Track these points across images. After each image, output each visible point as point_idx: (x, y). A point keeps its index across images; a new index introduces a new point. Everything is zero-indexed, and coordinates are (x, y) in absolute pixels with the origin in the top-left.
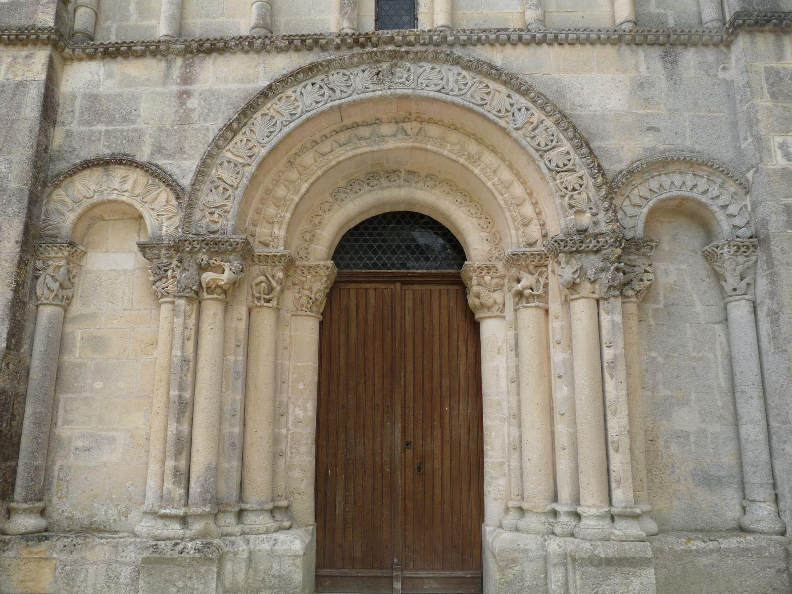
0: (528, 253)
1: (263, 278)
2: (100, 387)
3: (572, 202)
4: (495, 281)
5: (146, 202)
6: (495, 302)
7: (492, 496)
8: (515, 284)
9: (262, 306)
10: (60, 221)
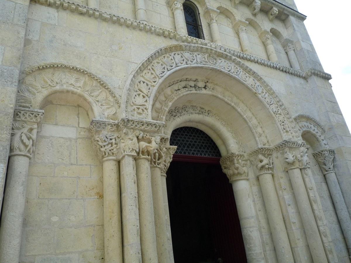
0: (266, 148)
2: (56, 220)
4: (243, 162)
5: (93, 96)
6: (244, 172)
8: (259, 163)
9: (156, 167)
10: (32, 98)
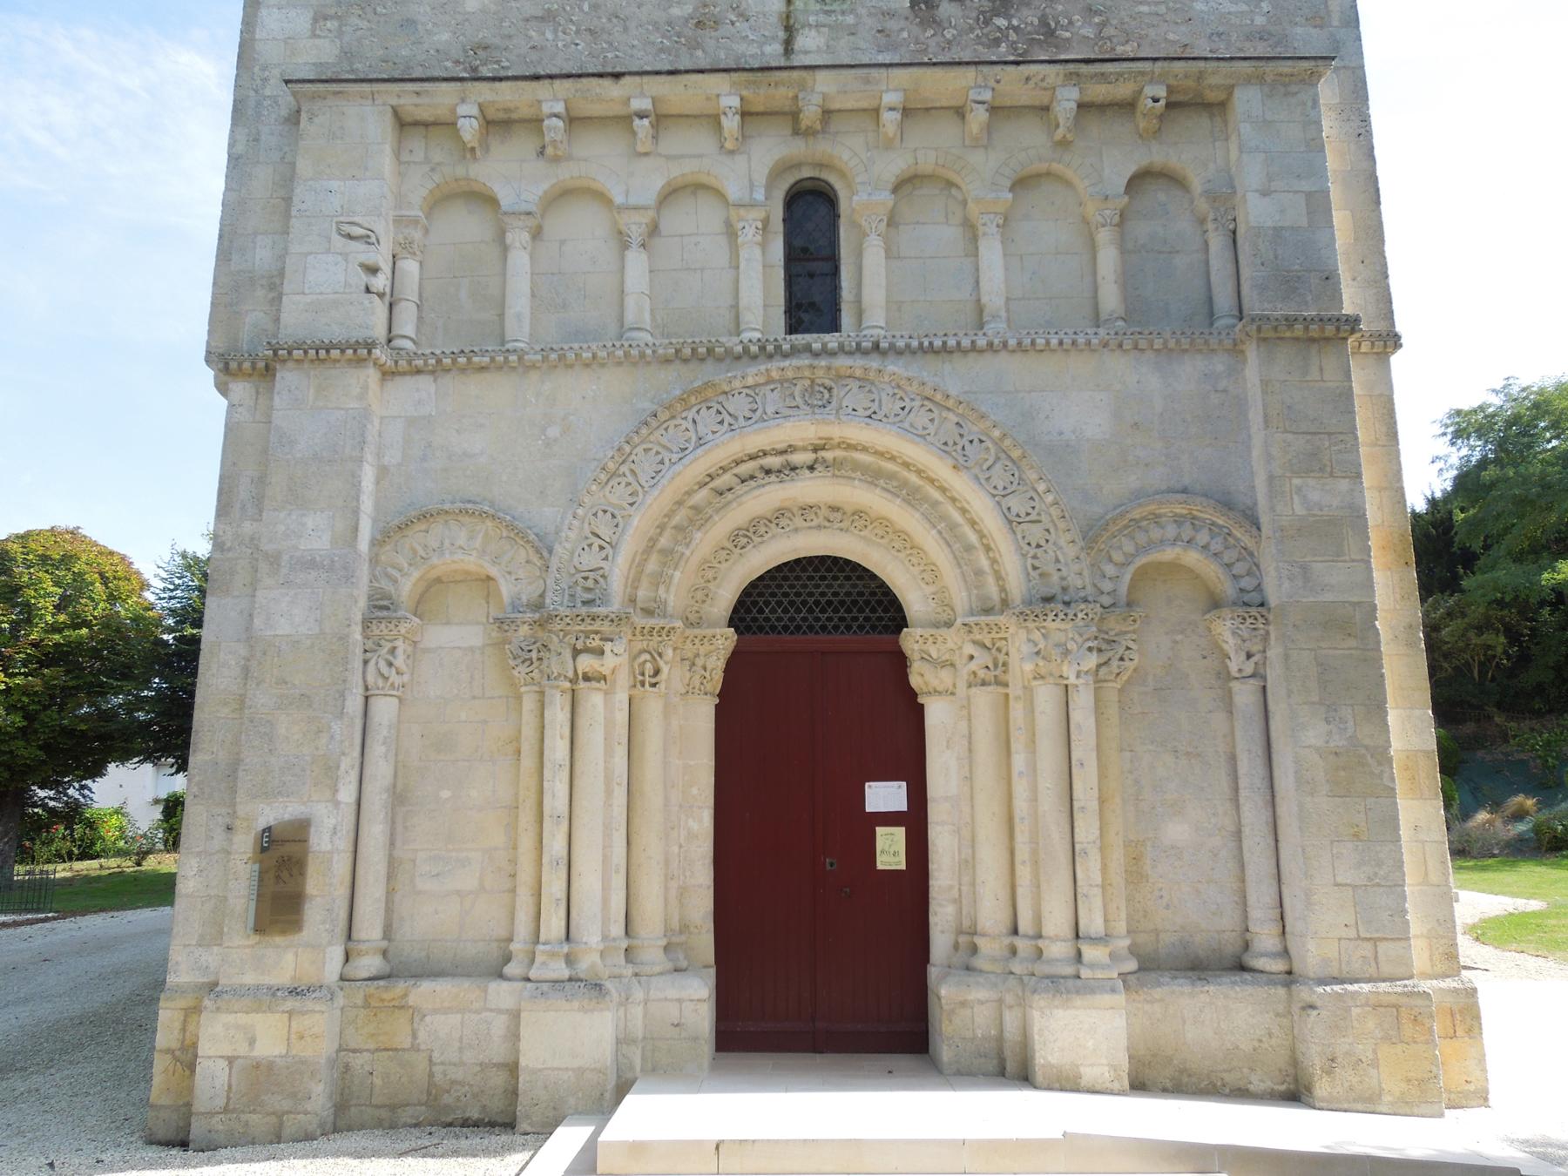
1: (647, 657)
3: (1037, 563)
7: (939, 928)
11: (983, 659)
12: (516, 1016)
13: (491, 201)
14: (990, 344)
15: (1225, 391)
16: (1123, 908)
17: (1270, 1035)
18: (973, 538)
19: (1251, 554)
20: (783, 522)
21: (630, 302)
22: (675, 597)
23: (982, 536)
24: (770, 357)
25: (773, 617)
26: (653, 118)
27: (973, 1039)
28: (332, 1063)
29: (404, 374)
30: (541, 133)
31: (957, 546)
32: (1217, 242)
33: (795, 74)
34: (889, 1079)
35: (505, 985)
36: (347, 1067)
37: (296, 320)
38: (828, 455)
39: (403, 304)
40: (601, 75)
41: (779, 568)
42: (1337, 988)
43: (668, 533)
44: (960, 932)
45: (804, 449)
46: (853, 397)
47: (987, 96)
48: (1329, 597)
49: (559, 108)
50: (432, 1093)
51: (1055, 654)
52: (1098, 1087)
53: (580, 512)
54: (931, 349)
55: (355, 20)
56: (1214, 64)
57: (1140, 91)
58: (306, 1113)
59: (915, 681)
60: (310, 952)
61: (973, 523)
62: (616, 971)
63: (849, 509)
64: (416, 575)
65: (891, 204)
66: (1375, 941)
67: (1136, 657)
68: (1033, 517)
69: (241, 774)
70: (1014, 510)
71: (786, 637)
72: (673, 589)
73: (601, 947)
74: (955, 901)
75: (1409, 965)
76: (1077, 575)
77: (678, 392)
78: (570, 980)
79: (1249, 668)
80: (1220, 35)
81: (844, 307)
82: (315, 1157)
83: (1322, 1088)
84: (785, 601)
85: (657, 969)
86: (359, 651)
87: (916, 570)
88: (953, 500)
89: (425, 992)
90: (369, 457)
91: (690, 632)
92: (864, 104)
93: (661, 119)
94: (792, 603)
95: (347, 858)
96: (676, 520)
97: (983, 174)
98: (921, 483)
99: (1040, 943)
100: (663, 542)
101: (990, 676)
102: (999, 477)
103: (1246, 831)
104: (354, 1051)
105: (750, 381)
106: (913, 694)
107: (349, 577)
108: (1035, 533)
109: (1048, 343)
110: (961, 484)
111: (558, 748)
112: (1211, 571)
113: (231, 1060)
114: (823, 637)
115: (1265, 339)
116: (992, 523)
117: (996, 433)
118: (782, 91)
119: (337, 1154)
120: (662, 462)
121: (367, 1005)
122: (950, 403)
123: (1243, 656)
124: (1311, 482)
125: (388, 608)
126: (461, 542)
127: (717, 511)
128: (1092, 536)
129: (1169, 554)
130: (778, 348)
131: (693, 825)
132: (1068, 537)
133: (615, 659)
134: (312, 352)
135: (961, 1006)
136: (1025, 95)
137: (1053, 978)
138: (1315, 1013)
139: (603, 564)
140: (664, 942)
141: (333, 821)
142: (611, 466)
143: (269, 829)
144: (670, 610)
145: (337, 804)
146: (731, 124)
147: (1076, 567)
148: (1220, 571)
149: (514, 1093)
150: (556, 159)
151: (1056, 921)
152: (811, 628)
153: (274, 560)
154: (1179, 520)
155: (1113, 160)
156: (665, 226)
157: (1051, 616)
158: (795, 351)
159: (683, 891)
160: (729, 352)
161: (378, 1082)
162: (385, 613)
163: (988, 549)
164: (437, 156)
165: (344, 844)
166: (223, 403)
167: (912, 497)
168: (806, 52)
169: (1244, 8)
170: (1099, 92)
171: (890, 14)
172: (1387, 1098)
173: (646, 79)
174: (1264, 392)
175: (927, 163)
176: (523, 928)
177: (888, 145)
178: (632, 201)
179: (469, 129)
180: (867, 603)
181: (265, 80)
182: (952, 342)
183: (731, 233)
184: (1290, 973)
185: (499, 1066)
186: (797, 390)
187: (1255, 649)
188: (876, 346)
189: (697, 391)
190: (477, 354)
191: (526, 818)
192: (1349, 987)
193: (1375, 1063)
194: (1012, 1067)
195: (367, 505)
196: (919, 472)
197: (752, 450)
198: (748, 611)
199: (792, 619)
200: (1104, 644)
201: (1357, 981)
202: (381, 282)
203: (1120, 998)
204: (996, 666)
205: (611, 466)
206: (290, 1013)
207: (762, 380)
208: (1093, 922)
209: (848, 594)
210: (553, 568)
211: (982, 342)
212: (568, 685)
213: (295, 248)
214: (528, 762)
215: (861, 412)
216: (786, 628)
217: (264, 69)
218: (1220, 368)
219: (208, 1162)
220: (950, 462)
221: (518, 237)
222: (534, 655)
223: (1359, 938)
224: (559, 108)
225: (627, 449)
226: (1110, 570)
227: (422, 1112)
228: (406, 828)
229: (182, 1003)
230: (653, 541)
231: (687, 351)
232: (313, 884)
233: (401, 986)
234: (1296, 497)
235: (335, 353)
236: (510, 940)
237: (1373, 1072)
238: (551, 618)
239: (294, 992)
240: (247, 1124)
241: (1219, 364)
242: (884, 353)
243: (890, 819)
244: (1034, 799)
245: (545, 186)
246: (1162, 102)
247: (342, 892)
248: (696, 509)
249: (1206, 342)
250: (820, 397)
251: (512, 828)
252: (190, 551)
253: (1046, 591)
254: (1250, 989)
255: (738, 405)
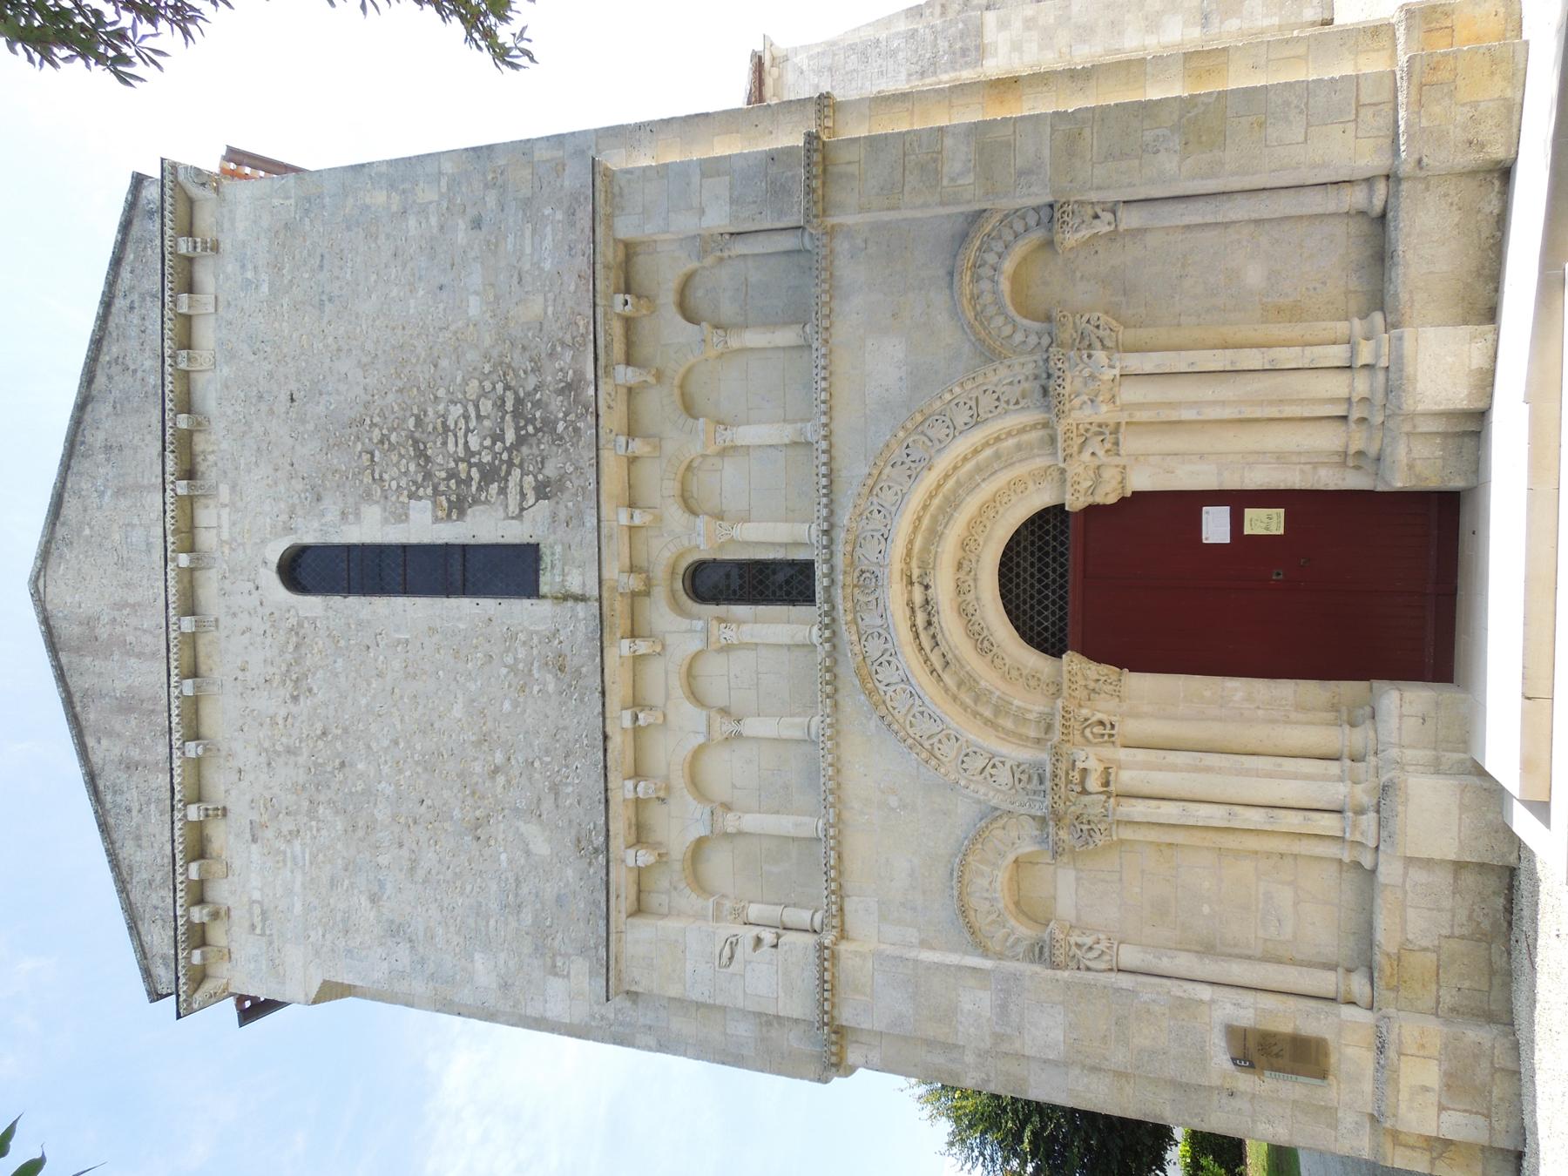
11: (1094, 445)
12: (1410, 861)
13: (700, 843)
14: (825, 437)
15: (866, 241)
16: (1323, 324)
17: (1446, 195)
18: (988, 452)
19: (1006, 216)
20: (970, 610)
21: (786, 734)
22: (1035, 705)
23: (987, 444)
24: (833, 620)
25: (1051, 619)
26: (637, 710)
27: (1443, 458)
28: (1447, 1022)
29: (843, 922)
30: (646, 801)
31: (996, 466)
32: (740, 248)
33: (605, 595)
34: (1479, 532)
35: (1381, 869)
36: (1453, 1010)
37: (799, 1005)
38: (916, 573)
39: (785, 918)
40: (605, 750)
41: (1009, 613)
42: (1402, 140)
43: (981, 709)
44: (1344, 464)
45: (910, 592)
46: (869, 552)
47: (622, 440)
48: (1046, 152)
49: (630, 784)
50: (1481, 937)
51: (1093, 386)
52: (1491, 353)
53: (963, 783)
54: (829, 486)
55: (556, 943)
56: (598, 256)
57: (618, 315)
58: (1493, 1047)
59: (1112, 499)
60: (1347, 1034)
61: (976, 452)
62: (1372, 771)
63: (960, 554)
64: (1013, 922)
65: (706, 518)
66: (1359, 106)
67: (1095, 315)
68: (973, 404)
69: (1184, 1080)
70: (968, 420)
71: (1069, 608)
72: (1029, 707)
73: (1349, 783)
74: (1315, 468)
75: (1381, 75)
76: (1024, 367)
77: (863, 697)
78: (1378, 812)
79: (1108, 216)
80: (571, 249)
81: (790, 557)
82: (1533, 1041)
83: (1498, 152)
84: (1037, 608)
85: (1371, 734)
86: (1079, 974)
87: (1014, 498)
88: (955, 468)
89: (1386, 936)
90: (912, 954)
91: (1065, 693)
92: (626, 538)
93: (637, 703)
94: (1039, 602)
95: (1262, 997)
96: (969, 701)
97: (687, 442)
98: (940, 496)
99: (1355, 399)
100: (988, 713)
101: (1110, 438)
102: (939, 432)
103: (1255, 216)
104: (1438, 1002)
105: (855, 638)
106: (1123, 500)
107: (1016, 977)
108: (987, 401)
109: (824, 390)
110: (943, 463)
111: (1169, 812)
112: (1020, 249)
113: (1442, 1108)
114: (1070, 577)
115: (824, 211)
116: (977, 436)
117: (901, 434)
118: (617, 605)
119: (1532, 1023)
120: (922, 713)
121: (1396, 989)
122: (875, 472)
123: (1096, 222)
124: (946, 169)
125: (1042, 948)
126: (985, 883)
127: (962, 667)
128: (989, 353)
129: (1005, 286)
130: (827, 614)
131: (1239, 695)
132: (990, 374)
133: (1091, 758)
134: (826, 994)
135: (1413, 466)
136: (621, 407)
137: (1388, 391)
138: (1425, 160)
139: (1008, 766)
140: (1347, 727)
141: (1228, 1006)
142: (924, 755)
143: (1234, 1060)
144: (1047, 710)
145: (1212, 1001)
146: (643, 647)
147: (1017, 368)
148: (1020, 243)
149: (1482, 865)
150: (668, 789)
151: (1336, 385)
152: (1062, 587)
153: (999, 1038)
154: (976, 279)
155: (671, 334)
156: (722, 703)
157: (1060, 390)
158: (829, 600)
159: (1299, 707)
160: (829, 655)
161: (1467, 984)
162: (1046, 950)
163: (998, 439)
164: (664, 883)
165: (1249, 998)
166: (861, 1071)
167: (952, 503)
168: (584, 584)
169: (549, 228)
170: (618, 349)
171: (554, 515)
172: (1509, 93)
173: (608, 715)
174: (869, 210)
175: (672, 487)
176: (1332, 850)
177: (659, 519)
178: (703, 728)
179: (645, 857)
180: (1040, 538)
181: (602, 1018)
182: (823, 470)
183: (727, 649)
184: (1388, 177)
185: (1456, 879)
186: (863, 599)
187: (1090, 212)
188: (826, 532)
189: (863, 682)
190: (828, 861)
191: (1230, 841)
192: (1402, 128)
193: (1475, 105)
194: (1471, 427)
195: (953, 959)
196: (931, 497)
197: (911, 636)
198: (1046, 640)
199: (1054, 603)
200: (1085, 344)
201: (1396, 122)
202: (768, 936)
203: (1408, 332)
204: (1101, 433)
205: (924, 755)
206: (1400, 1054)
207: (854, 629)
208: (1338, 354)
209: (1032, 554)
210: (1011, 808)
211: (824, 445)
212: (1112, 800)
213: (740, 1004)
214: (1179, 837)
215: (882, 547)
216: (1061, 608)
217: (593, 1017)
218: (846, 245)
219: (1535, 1133)
220: (925, 472)
221: (731, 822)
222: (1085, 827)
223: (1355, 120)
224: (630, 784)
225: (910, 741)
226: (1019, 337)
227: (1497, 948)
228: (1235, 945)
229: (1388, 1146)
230: (987, 722)
231: (828, 689)
232: (1285, 1027)
233: (1379, 958)
234: (960, 182)
235: (827, 976)
236: (1340, 861)
237: (1482, 106)
238: (1054, 812)
239: (1381, 1049)
240: (1501, 1099)
241: (842, 246)
242: (832, 526)
243: (1237, 522)
244: (1223, 403)
245: (689, 798)
246: (628, 297)
247: (1292, 1002)
248: (960, 684)
249: (825, 257)
250: (868, 580)
251: (1237, 854)
252: (947, 1139)
253: (1038, 394)
254: (1402, 215)
255: (874, 648)
